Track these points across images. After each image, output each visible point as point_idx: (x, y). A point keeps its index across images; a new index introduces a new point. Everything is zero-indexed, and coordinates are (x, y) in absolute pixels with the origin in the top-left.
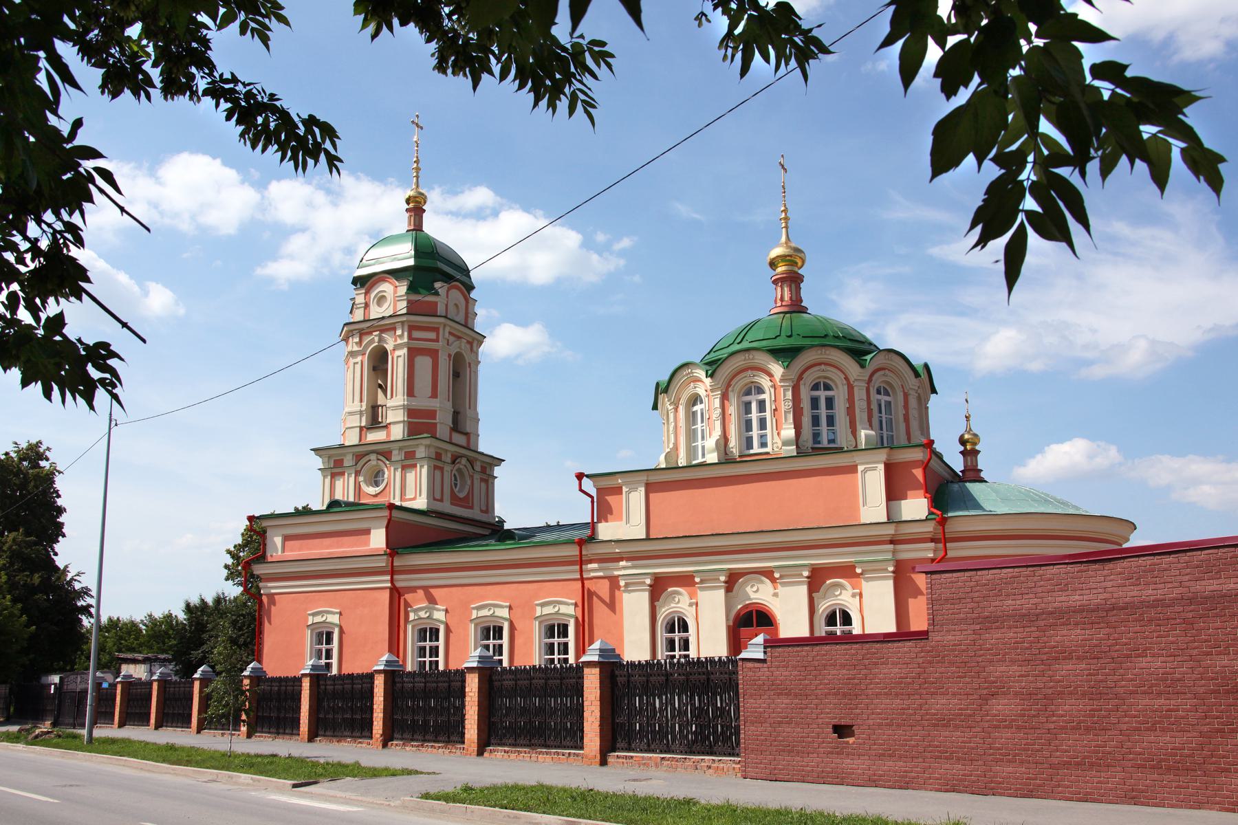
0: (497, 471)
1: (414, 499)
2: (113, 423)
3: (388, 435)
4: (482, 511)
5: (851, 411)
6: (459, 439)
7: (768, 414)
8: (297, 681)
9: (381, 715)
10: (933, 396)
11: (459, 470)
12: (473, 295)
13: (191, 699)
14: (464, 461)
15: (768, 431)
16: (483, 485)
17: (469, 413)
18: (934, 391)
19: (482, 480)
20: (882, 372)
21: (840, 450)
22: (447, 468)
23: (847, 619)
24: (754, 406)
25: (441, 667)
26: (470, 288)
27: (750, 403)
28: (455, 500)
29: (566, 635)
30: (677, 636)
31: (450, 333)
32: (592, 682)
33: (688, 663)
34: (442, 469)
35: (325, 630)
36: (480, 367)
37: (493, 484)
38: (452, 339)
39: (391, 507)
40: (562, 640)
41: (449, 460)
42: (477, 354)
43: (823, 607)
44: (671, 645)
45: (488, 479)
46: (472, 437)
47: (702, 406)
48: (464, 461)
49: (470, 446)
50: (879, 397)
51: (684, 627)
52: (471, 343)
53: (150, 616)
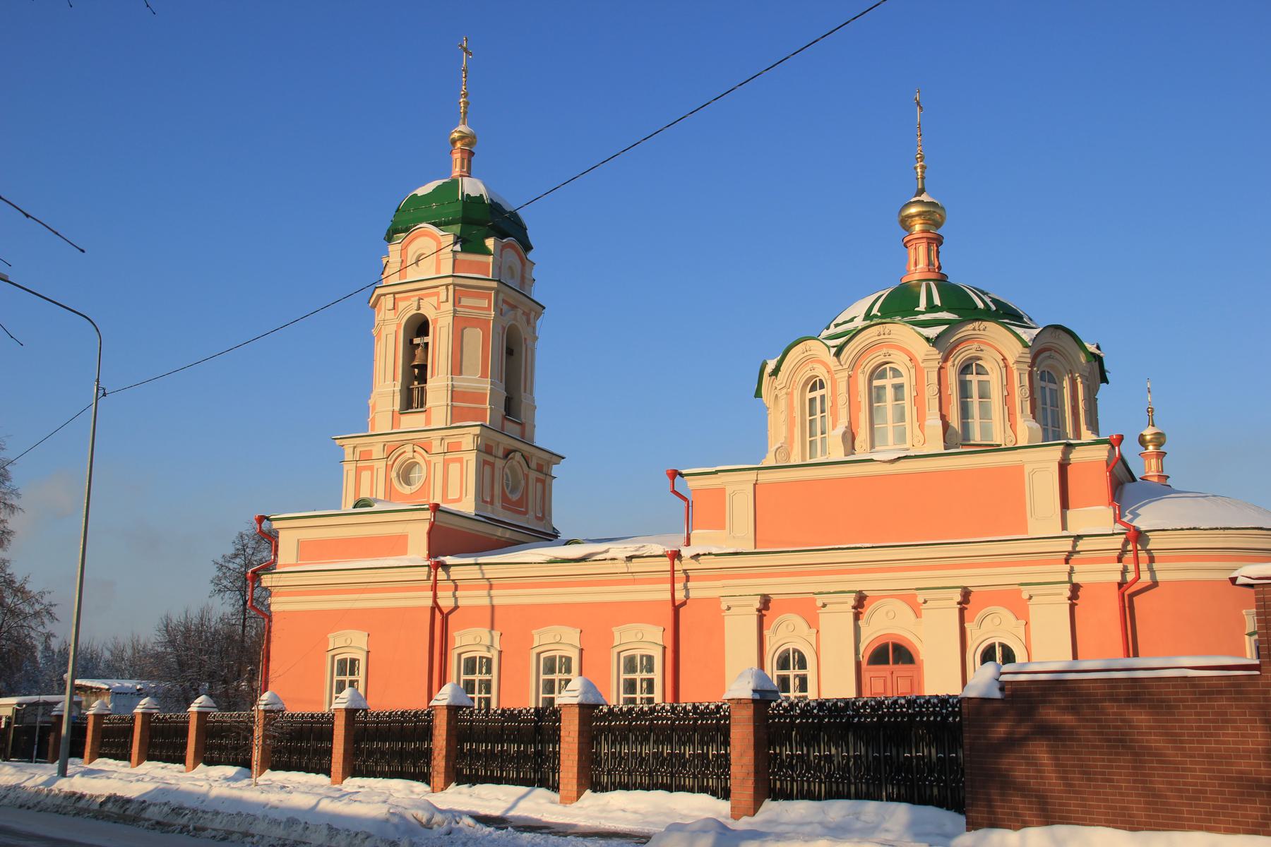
0: (555, 470)
1: (459, 500)
2: (101, 392)
3: (428, 421)
4: (537, 518)
5: (1007, 399)
6: (511, 428)
7: (907, 403)
8: (330, 720)
9: (443, 763)
10: (1103, 386)
11: (512, 469)
12: (531, 256)
13: (85, 736)
14: (518, 455)
15: (907, 423)
16: (539, 485)
17: (524, 397)
18: (1104, 380)
19: (538, 480)
20: (1047, 354)
21: (997, 449)
22: (499, 463)
23: (1009, 656)
24: (889, 393)
25: (494, 705)
26: (528, 247)
27: (883, 387)
28: (507, 504)
29: (651, 670)
30: (792, 673)
31: (504, 301)
32: (570, 730)
33: (652, 710)
34: (492, 465)
35: (349, 656)
36: (538, 344)
37: (550, 486)
38: (505, 307)
39: (436, 508)
40: (802, 672)
41: (500, 453)
42: (534, 328)
43: (978, 639)
44: (631, 686)
45: (544, 477)
46: (527, 429)
47: (823, 392)
48: (518, 455)
49: (525, 436)
50: (1043, 384)
51: (802, 663)
52: (527, 315)
53: (116, 638)
